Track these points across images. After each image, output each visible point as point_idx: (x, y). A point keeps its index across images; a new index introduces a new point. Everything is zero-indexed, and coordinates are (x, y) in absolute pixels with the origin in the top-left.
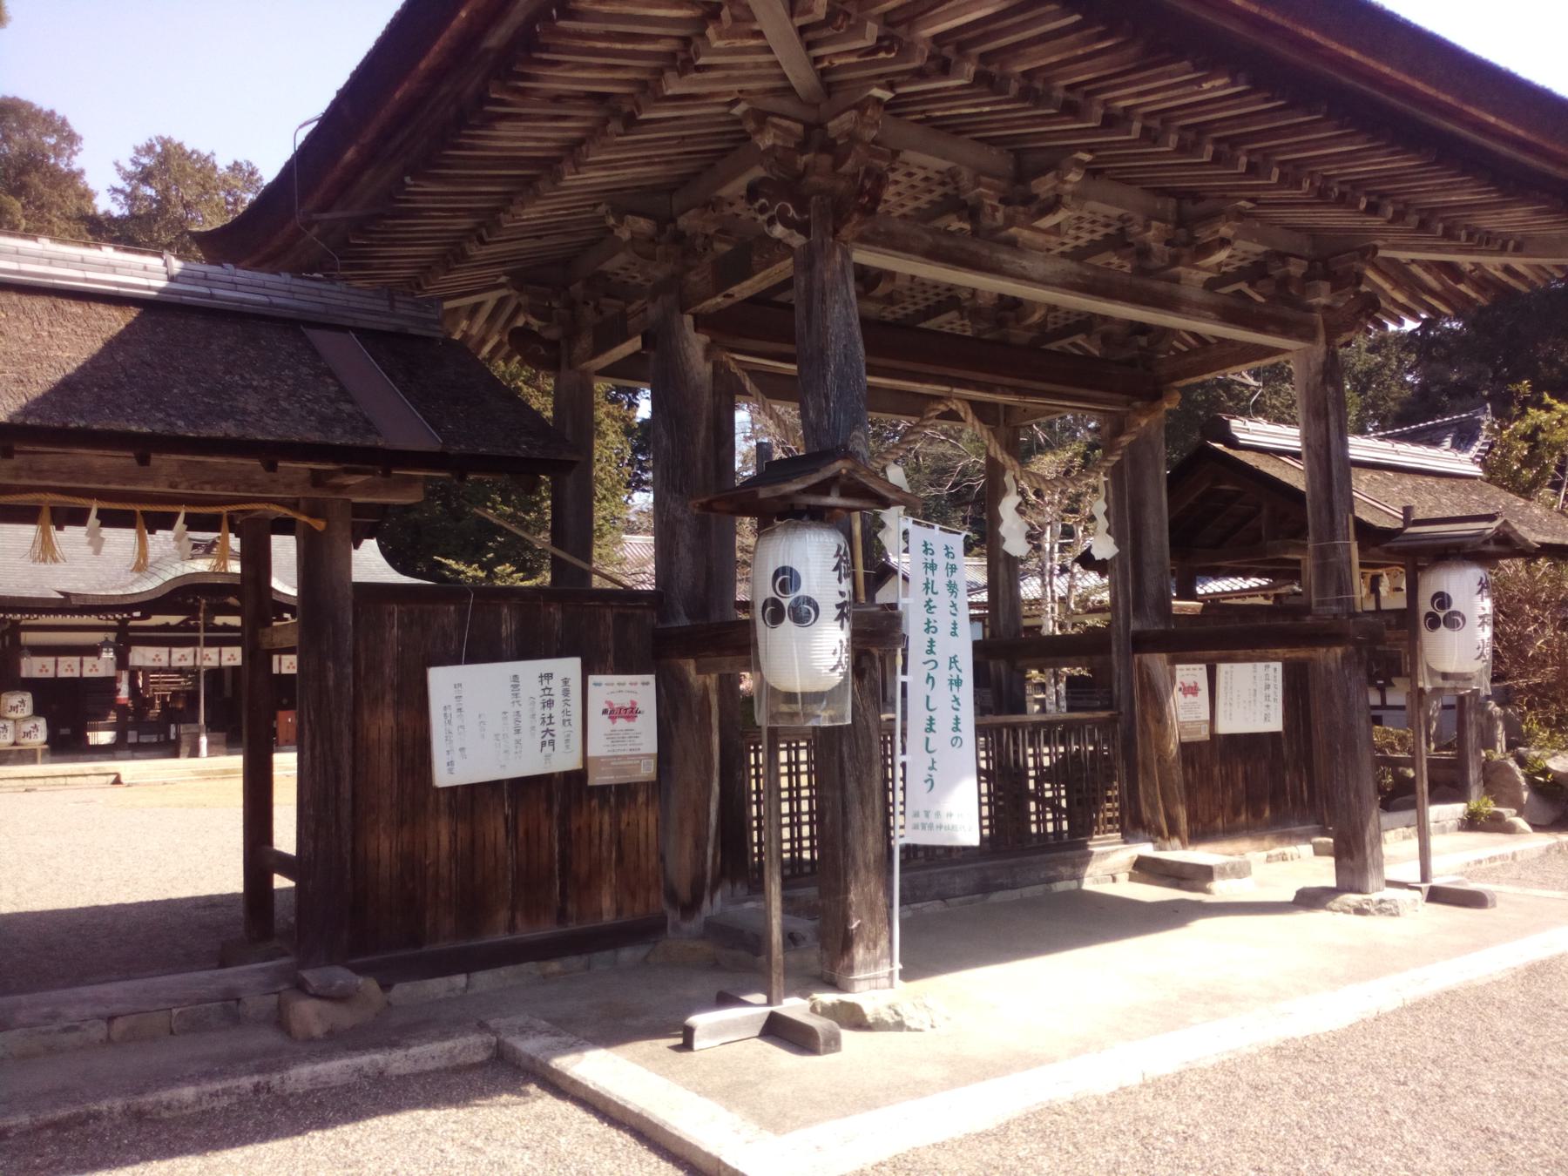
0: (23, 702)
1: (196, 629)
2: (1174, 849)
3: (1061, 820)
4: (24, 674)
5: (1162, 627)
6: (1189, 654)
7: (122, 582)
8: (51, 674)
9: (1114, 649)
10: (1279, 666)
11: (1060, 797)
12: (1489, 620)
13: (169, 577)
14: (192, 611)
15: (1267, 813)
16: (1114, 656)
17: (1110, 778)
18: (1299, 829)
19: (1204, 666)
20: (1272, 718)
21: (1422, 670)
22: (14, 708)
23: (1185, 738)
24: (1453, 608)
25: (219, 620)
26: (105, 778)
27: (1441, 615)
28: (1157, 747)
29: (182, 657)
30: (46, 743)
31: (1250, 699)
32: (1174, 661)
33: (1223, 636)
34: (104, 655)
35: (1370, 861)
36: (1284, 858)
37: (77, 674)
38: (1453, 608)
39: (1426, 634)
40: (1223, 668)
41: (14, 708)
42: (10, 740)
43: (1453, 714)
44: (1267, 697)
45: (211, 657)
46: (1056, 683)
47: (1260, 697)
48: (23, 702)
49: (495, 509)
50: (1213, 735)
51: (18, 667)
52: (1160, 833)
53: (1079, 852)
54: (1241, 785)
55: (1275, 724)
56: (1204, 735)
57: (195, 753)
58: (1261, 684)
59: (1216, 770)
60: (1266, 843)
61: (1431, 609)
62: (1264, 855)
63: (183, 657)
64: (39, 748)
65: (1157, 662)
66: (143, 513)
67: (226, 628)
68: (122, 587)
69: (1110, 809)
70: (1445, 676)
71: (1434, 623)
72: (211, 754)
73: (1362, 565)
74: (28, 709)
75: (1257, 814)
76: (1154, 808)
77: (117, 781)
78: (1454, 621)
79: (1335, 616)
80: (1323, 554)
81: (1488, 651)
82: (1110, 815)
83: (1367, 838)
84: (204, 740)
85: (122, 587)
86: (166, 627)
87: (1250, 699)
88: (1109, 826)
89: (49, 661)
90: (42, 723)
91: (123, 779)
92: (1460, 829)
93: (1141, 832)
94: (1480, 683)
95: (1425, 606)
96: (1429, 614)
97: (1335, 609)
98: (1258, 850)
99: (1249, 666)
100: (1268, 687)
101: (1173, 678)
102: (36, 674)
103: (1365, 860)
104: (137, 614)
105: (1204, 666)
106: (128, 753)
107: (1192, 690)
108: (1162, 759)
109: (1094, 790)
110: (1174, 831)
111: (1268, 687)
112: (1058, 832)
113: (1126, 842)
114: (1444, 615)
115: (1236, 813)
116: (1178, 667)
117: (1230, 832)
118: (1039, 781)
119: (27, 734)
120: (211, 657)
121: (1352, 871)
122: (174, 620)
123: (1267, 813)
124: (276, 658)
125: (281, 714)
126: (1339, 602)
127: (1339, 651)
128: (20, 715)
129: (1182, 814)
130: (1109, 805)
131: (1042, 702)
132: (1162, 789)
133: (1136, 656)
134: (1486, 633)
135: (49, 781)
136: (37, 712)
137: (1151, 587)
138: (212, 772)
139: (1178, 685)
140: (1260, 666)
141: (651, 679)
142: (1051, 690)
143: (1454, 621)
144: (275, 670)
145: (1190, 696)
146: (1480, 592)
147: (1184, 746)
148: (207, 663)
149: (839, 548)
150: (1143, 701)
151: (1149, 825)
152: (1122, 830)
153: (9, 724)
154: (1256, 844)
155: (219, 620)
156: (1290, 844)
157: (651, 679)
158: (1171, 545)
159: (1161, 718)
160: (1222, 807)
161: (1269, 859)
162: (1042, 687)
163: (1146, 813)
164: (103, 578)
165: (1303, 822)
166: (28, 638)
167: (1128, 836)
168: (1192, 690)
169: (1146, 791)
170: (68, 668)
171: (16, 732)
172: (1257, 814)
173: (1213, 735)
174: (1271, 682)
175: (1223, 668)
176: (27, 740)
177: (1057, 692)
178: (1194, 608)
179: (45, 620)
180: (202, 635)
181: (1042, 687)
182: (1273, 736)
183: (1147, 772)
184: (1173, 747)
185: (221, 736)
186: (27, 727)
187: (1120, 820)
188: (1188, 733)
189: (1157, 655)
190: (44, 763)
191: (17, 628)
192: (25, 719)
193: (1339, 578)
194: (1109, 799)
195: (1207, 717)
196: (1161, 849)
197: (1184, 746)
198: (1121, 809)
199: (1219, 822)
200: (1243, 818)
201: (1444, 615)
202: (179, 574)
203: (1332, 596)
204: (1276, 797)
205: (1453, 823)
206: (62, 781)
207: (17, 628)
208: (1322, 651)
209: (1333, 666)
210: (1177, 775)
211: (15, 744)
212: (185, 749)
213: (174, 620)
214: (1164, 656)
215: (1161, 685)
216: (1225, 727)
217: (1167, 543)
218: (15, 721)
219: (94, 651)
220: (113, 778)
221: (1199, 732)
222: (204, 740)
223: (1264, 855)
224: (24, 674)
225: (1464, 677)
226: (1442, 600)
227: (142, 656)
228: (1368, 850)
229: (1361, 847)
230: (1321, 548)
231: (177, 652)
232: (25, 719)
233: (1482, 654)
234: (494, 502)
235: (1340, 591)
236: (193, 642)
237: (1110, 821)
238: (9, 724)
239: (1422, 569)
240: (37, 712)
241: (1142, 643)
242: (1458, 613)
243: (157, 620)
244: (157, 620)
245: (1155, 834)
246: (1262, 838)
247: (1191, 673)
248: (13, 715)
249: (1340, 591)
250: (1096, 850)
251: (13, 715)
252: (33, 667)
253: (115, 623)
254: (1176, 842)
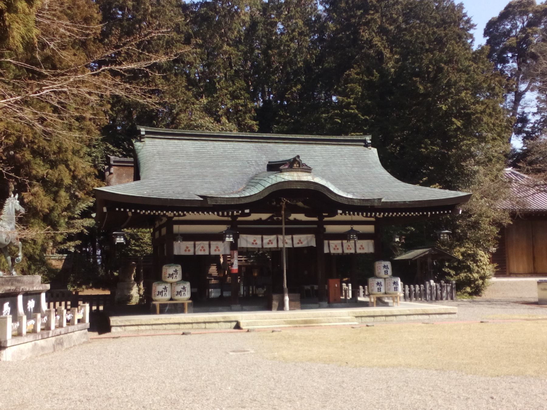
0: (184, 288)
1: (280, 223)
4: (176, 252)
7: (236, 189)
8: (191, 253)
13: (268, 185)
14: (276, 211)
22: (171, 276)
25: (293, 217)
26: (229, 324)
29: (270, 242)
30: (190, 299)
34: (227, 239)
37: (207, 253)
41: (171, 276)
42: (168, 297)
45: (286, 242)
48: (176, 271)
49: (426, 148)
51: (171, 248)
57: (281, 307)
63: (270, 242)
64: (187, 302)
67: (296, 222)
68: (238, 192)
72: (292, 308)
74: (179, 277)
77: (238, 326)
84: (287, 298)
85: (238, 192)
86: (260, 222)
89: (190, 244)
90: (188, 285)
91: (242, 325)
102: (183, 253)
104: (247, 211)
106: (238, 306)
119: (179, 293)
120: (286, 242)
122: (265, 216)
124: (326, 242)
125: (331, 281)
128: (174, 280)
135: (195, 326)
136: (185, 278)
138: (297, 322)
141: (373, 241)
144: (326, 251)
148: (286, 246)
153: (168, 286)
155: (293, 217)
157: (373, 241)
164: (225, 188)
166: (177, 228)
170: (202, 248)
171: (172, 291)
176: (178, 297)
179: (190, 216)
180: (284, 226)
185: (298, 295)
186: (179, 288)
190: (189, 312)
191: (171, 222)
192: (177, 283)
202: (274, 182)
206: (203, 326)
207: (171, 222)
211: (171, 299)
212: (275, 303)
213: (265, 216)
218: (171, 284)
219: (220, 237)
220: (234, 324)
222: (287, 298)
224: (176, 252)
227: (248, 241)
231: (267, 238)
232: (177, 283)
234: (426, 144)
236: (278, 232)
238: (168, 286)
240: (185, 278)
243: (255, 217)
244: (255, 217)
248: (170, 280)
251: (170, 280)
252: (181, 248)
253: (373, 219)
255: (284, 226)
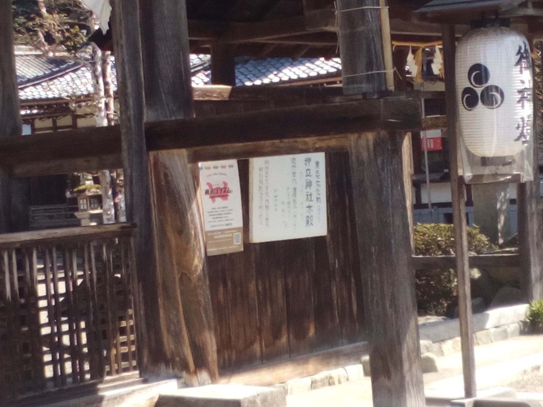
2: (201, 384)
3: (62, 361)
5: (180, 117)
6: (211, 149)
9: (124, 145)
10: (321, 157)
11: (60, 334)
12: (528, 94)
15: (312, 332)
16: (125, 154)
17: (125, 305)
18: (347, 347)
19: (234, 162)
20: (315, 221)
21: (462, 155)
23: (213, 251)
24: (490, 83)
27: (479, 90)
28: (179, 264)
31: (287, 198)
32: (196, 158)
33: (254, 127)
35: (408, 378)
36: (330, 382)
38: (490, 83)
39: (464, 113)
40: (257, 164)
43: (515, 207)
44: (309, 196)
46: (115, 195)
47: (301, 198)
50: (248, 245)
52: (185, 367)
53: (86, 399)
54: (281, 301)
55: (319, 228)
56: (237, 245)
58: (301, 182)
59: (252, 287)
60: (311, 366)
61: (469, 85)
62: (308, 380)
65: (176, 159)
66: (412, 47)
69: (124, 344)
70: (485, 161)
71: (471, 101)
73: (394, 38)
75: (300, 334)
76: (177, 337)
78: (490, 97)
79: (364, 94)
80: (351, 21)
81: (528, 131)
82: (124, 350)
83: (405, 354)
87: (287, 198)
88: (124, 364)
91: (350, 380)
92: (523, 333)
93: (163, 367)
94: (522, 168)
95: (463, 81)
96: (467, 90)
97: (365, 87)
98: (301, 375)
99: (285, 160)
100: (309, 184)
101: (196, 178)
103: (403, 378)
105: (234, 162)
107: (222, 192)
108: (185, 278)
109: (104, 322)
110: (201, 363)
111: (309, 184)
112: (78, 373)
113: (145, 381)
114: (482, 92)
115: (276, 335)
116: (200, 164)
117: (271, 358)
118: (54, 320)
121: (390, 391)
123: (312, 332)
126: (369, 79)
127: (370, 136)
129: (210, 342)
130: (123, 338)
131: (98, 218)
132: (186, 313)
133: (152, 154)
134: (527, 110)
137: (166, 68)
139: (203, 186)
140: (301, 157)
142: (109, 203)
143: (490, 97)
145: (218, 200)
146: (519, 63)
147: (212, 261)
149: (520, 48)
150: (161, 209)
151: (173, 360)
152: (140, 367)
154: (300, 369)
156: (337, 365)
158: (190, 15)
159: (182, 229)
160: (260, 331)
161: (314, 385)
162: (98, 200)
163: (169, 345)
165: (352, 340)
167: (148, 374)
168: (222, 192)
169: (169, 320)
172: (300, 334)
173: (248, 245)
174: (314, 179)
175: (257, 164)
177: (116, 205)
178: (220, 93)
181: (98, 200)
182: (318, 241)
183: (169, 296)
184: (198, 263)
187: (138, 355)
188: (218, 245)
189: (175, 151)
193: (369, 50)
194: (123, 331)
195: (239, 223)
196: (186, 385)
197: (212, 261)
198: (139, 342)
199: (257, 347)
200: (284, 339)
201: (482, 92)
203: (362, 73)
204: (322, 312)
205: (514, 327)
208: (353, 137)
209: (365, 155)
210: (204, 295)
214: (184, 152)
215: (182, 187)
216: (259, 235)
217: (183, 13)
221: (230, 243)
223: (308, 380)
225: (503, 161)
226: (479, 73)
228: (406, 366)
229: (398, 363)
230: (349, 14)
233: (522, 135)
235: (370, 66)
237: (125, 357)
239: (458, 39)
241: (158, 137)
242: (497, 88)
245: (180, 368)
246: (306, 361)
247: (219, 172)
249: (370, 66)
250: (107, 394)
254: (204, 375)
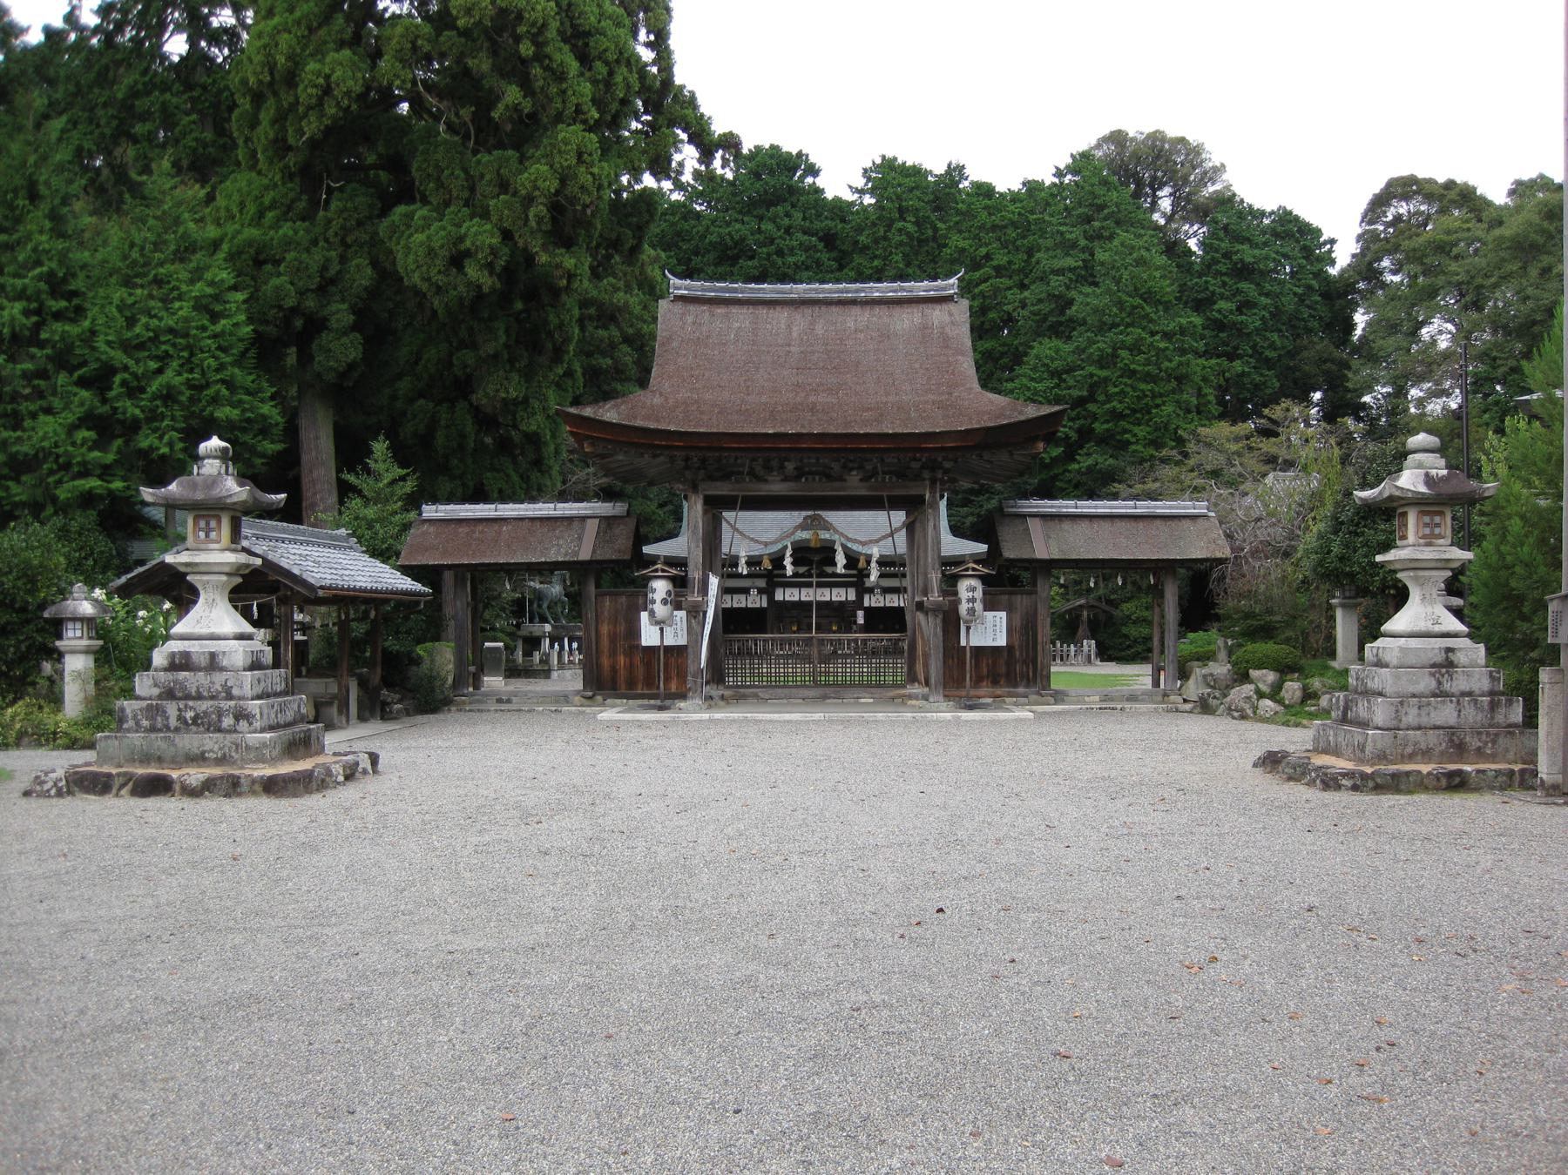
255: (814, 580)
